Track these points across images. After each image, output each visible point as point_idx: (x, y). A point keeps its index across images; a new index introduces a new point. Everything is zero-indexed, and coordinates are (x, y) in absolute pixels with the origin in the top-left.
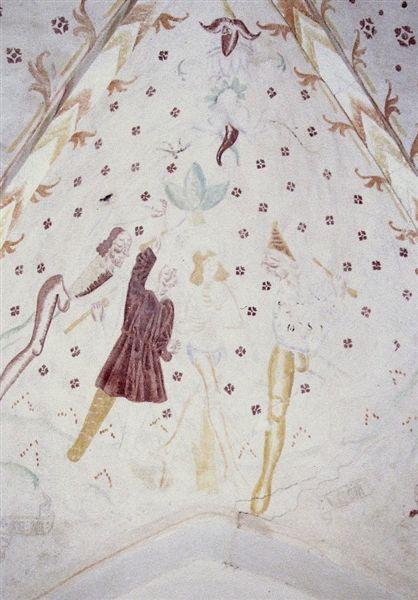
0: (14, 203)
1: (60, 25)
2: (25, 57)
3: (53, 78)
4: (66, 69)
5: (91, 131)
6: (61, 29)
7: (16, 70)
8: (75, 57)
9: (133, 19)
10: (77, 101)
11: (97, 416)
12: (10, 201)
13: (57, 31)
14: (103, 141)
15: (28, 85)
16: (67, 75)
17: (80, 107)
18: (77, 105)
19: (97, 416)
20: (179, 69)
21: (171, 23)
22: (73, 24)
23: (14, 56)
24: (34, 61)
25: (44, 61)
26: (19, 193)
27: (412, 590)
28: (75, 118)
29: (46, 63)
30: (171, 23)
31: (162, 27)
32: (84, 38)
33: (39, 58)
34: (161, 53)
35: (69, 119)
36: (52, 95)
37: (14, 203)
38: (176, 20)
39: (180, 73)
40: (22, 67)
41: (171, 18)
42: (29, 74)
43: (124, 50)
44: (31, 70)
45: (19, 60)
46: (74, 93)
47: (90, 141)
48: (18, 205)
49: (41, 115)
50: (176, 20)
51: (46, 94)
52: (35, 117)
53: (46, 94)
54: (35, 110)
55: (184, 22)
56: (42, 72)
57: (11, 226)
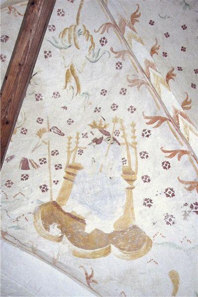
0: (179, 116)
1: (119, 66)
2: (126, 87)
3: (138, 77)
4: (136, 69)
5: (171, 69)
6: (121, 66)
7: (129, 92)
8: (133, 64)
9: (124, 29)
10: (148, 68)
11: (114, 125)
12: (178, 117)
13: (121, 68)
14: (180, 66)
15: (137, 89)
16: (139, 70)
17: (151, 67)
18: (150, 68)
19: (114, 125)
20: (162, 18)
21: (138, 14)
22: (120, 60)
23: (123, 91)
24: (128, 83)
25: (131, 79)
26: (176, 111)
27: (69, 186)
28: (155, 72)
29: (131, 78)
30: (138, 14)
31: (137, 19)
32: (127, 56)
33: (128, 80)
34: (150, 23)
35: (154, 73)
36: (144, 80)
37: (179, 116)
38: (137, 11)
39: (165, 18)
40: (129, 90)
41: (135, 13)
42: (133, 87)
43: (135, 37)
44: (131, 86)
45: (126, 90)
46: (144, 68)
47: (176, 72)
48: (182, 114)
49: (150, 88)
50: (137, 11)
51: (143, 83)
52: (150, 91)
53: (143, 83)
54: (147, 90)
55: (140, 8)
56: (134, 81)
57: (190, 121)
